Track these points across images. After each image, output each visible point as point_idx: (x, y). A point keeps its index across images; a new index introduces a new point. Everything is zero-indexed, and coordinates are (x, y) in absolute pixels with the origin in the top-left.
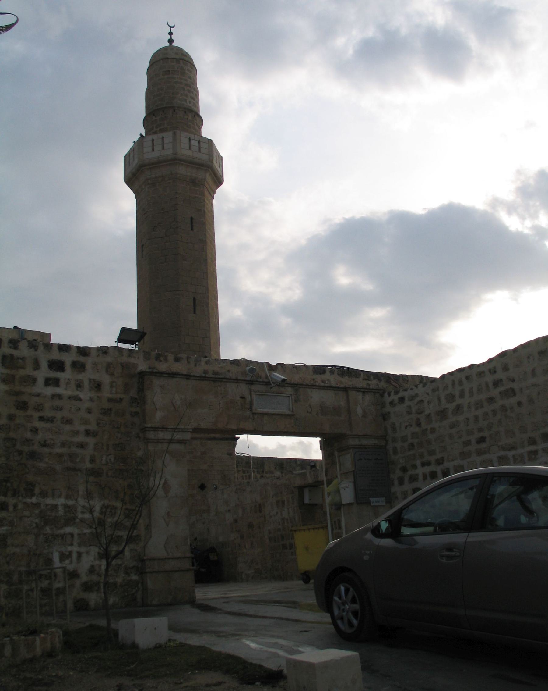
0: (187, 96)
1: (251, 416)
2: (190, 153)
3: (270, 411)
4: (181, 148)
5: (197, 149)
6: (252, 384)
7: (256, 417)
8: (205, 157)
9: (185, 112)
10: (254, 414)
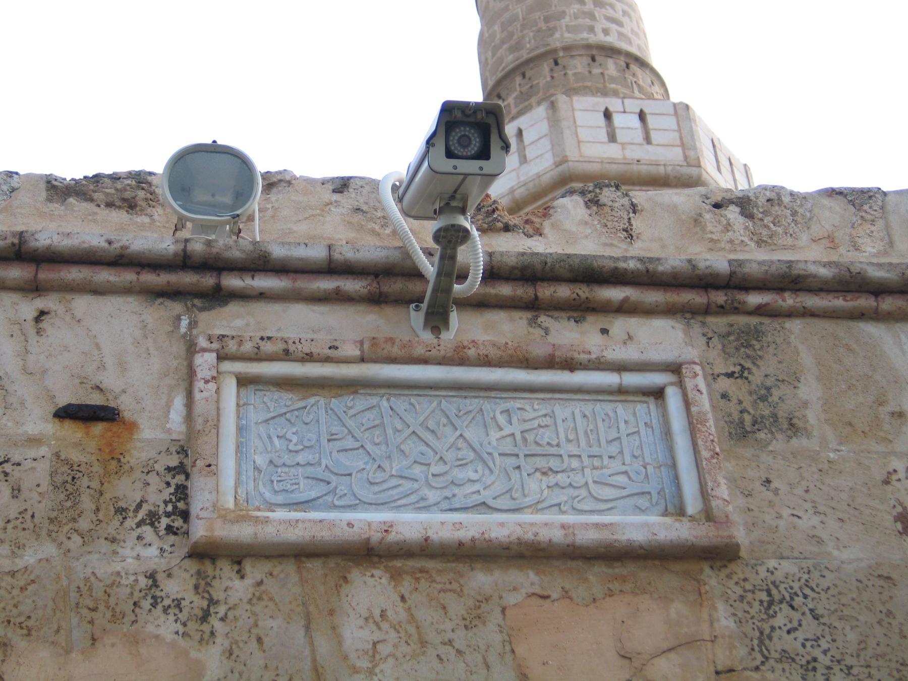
0: (592, 16)
1: (176, 587)
2: (613, 151)
3: (409, 524)
4: (579, 142)
5: (639, 136)
6: (218, 297)
7: (234, 587)
8: (674, 156)
9: (593, 59)
10: (205, 554)
